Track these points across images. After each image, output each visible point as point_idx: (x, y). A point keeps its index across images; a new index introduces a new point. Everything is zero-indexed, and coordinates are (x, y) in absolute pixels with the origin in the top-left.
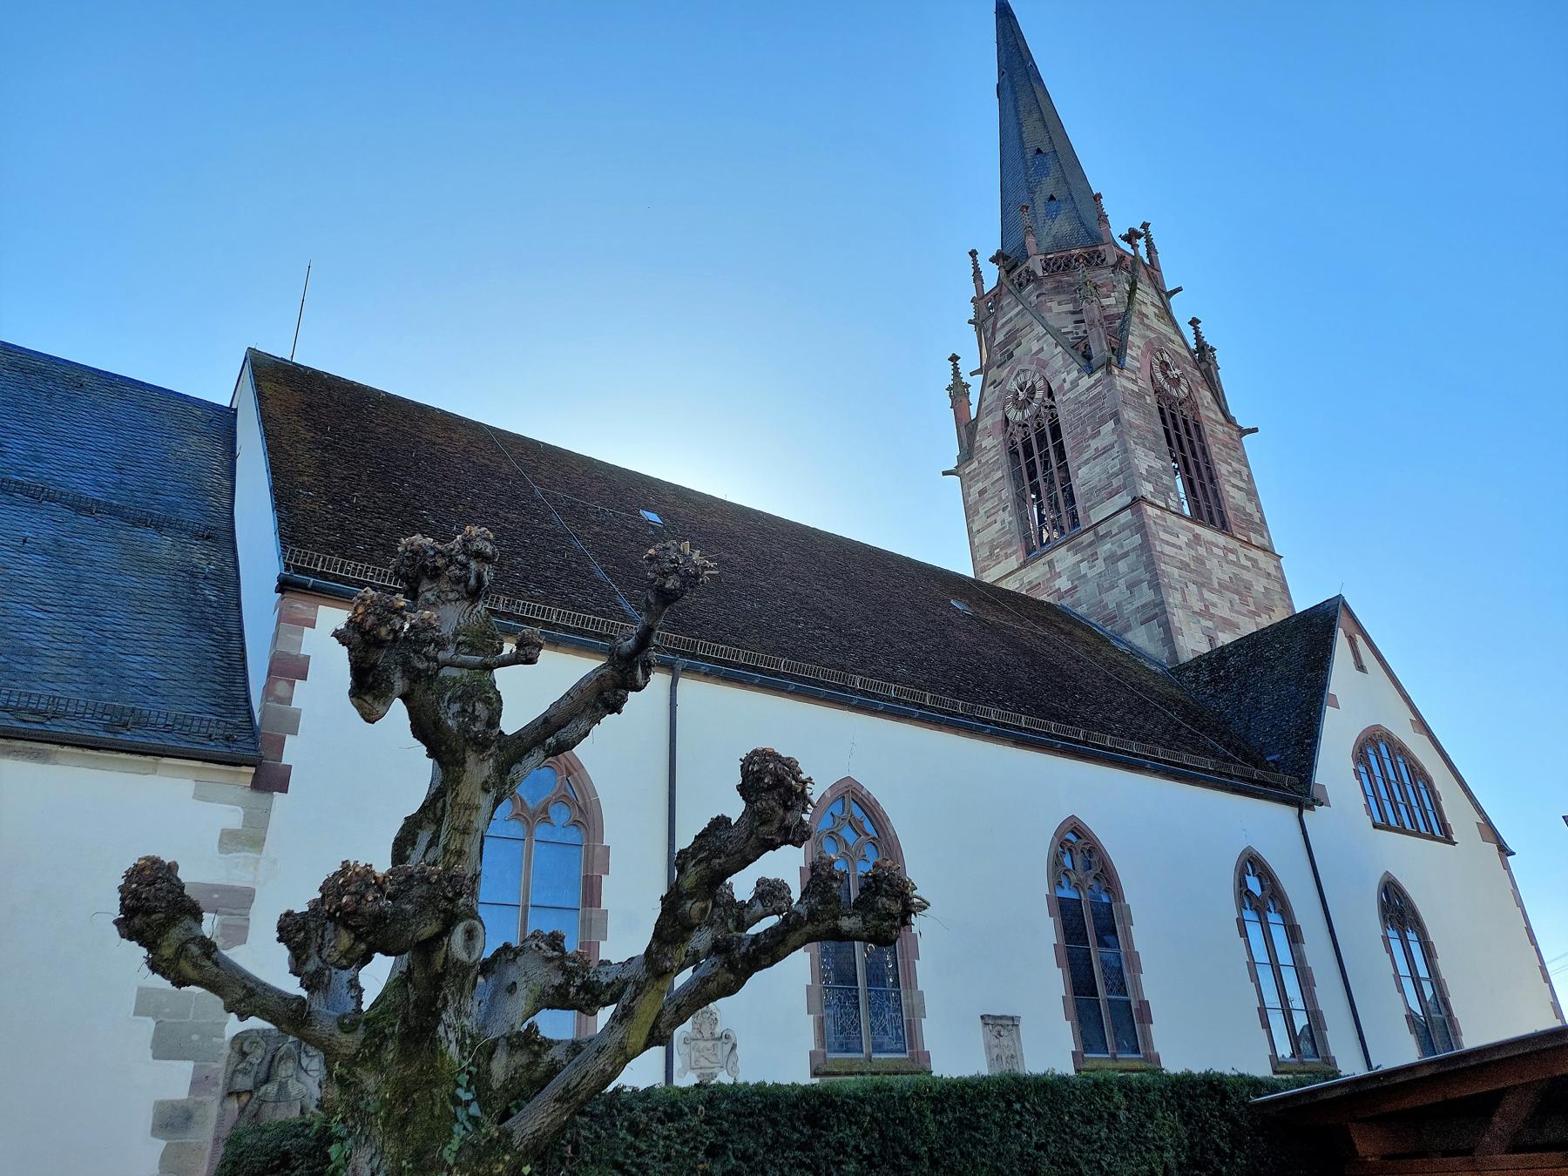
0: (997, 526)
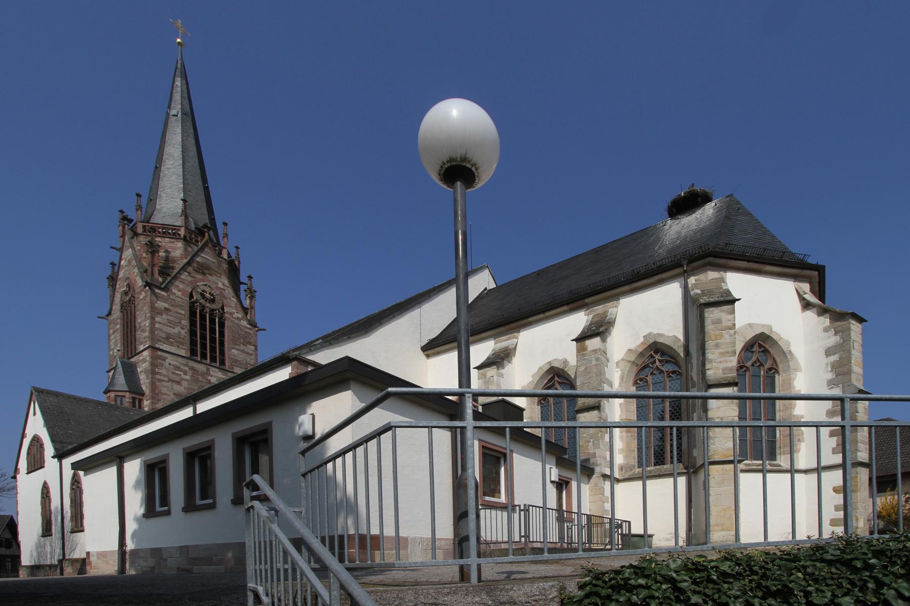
0: (176, 331)
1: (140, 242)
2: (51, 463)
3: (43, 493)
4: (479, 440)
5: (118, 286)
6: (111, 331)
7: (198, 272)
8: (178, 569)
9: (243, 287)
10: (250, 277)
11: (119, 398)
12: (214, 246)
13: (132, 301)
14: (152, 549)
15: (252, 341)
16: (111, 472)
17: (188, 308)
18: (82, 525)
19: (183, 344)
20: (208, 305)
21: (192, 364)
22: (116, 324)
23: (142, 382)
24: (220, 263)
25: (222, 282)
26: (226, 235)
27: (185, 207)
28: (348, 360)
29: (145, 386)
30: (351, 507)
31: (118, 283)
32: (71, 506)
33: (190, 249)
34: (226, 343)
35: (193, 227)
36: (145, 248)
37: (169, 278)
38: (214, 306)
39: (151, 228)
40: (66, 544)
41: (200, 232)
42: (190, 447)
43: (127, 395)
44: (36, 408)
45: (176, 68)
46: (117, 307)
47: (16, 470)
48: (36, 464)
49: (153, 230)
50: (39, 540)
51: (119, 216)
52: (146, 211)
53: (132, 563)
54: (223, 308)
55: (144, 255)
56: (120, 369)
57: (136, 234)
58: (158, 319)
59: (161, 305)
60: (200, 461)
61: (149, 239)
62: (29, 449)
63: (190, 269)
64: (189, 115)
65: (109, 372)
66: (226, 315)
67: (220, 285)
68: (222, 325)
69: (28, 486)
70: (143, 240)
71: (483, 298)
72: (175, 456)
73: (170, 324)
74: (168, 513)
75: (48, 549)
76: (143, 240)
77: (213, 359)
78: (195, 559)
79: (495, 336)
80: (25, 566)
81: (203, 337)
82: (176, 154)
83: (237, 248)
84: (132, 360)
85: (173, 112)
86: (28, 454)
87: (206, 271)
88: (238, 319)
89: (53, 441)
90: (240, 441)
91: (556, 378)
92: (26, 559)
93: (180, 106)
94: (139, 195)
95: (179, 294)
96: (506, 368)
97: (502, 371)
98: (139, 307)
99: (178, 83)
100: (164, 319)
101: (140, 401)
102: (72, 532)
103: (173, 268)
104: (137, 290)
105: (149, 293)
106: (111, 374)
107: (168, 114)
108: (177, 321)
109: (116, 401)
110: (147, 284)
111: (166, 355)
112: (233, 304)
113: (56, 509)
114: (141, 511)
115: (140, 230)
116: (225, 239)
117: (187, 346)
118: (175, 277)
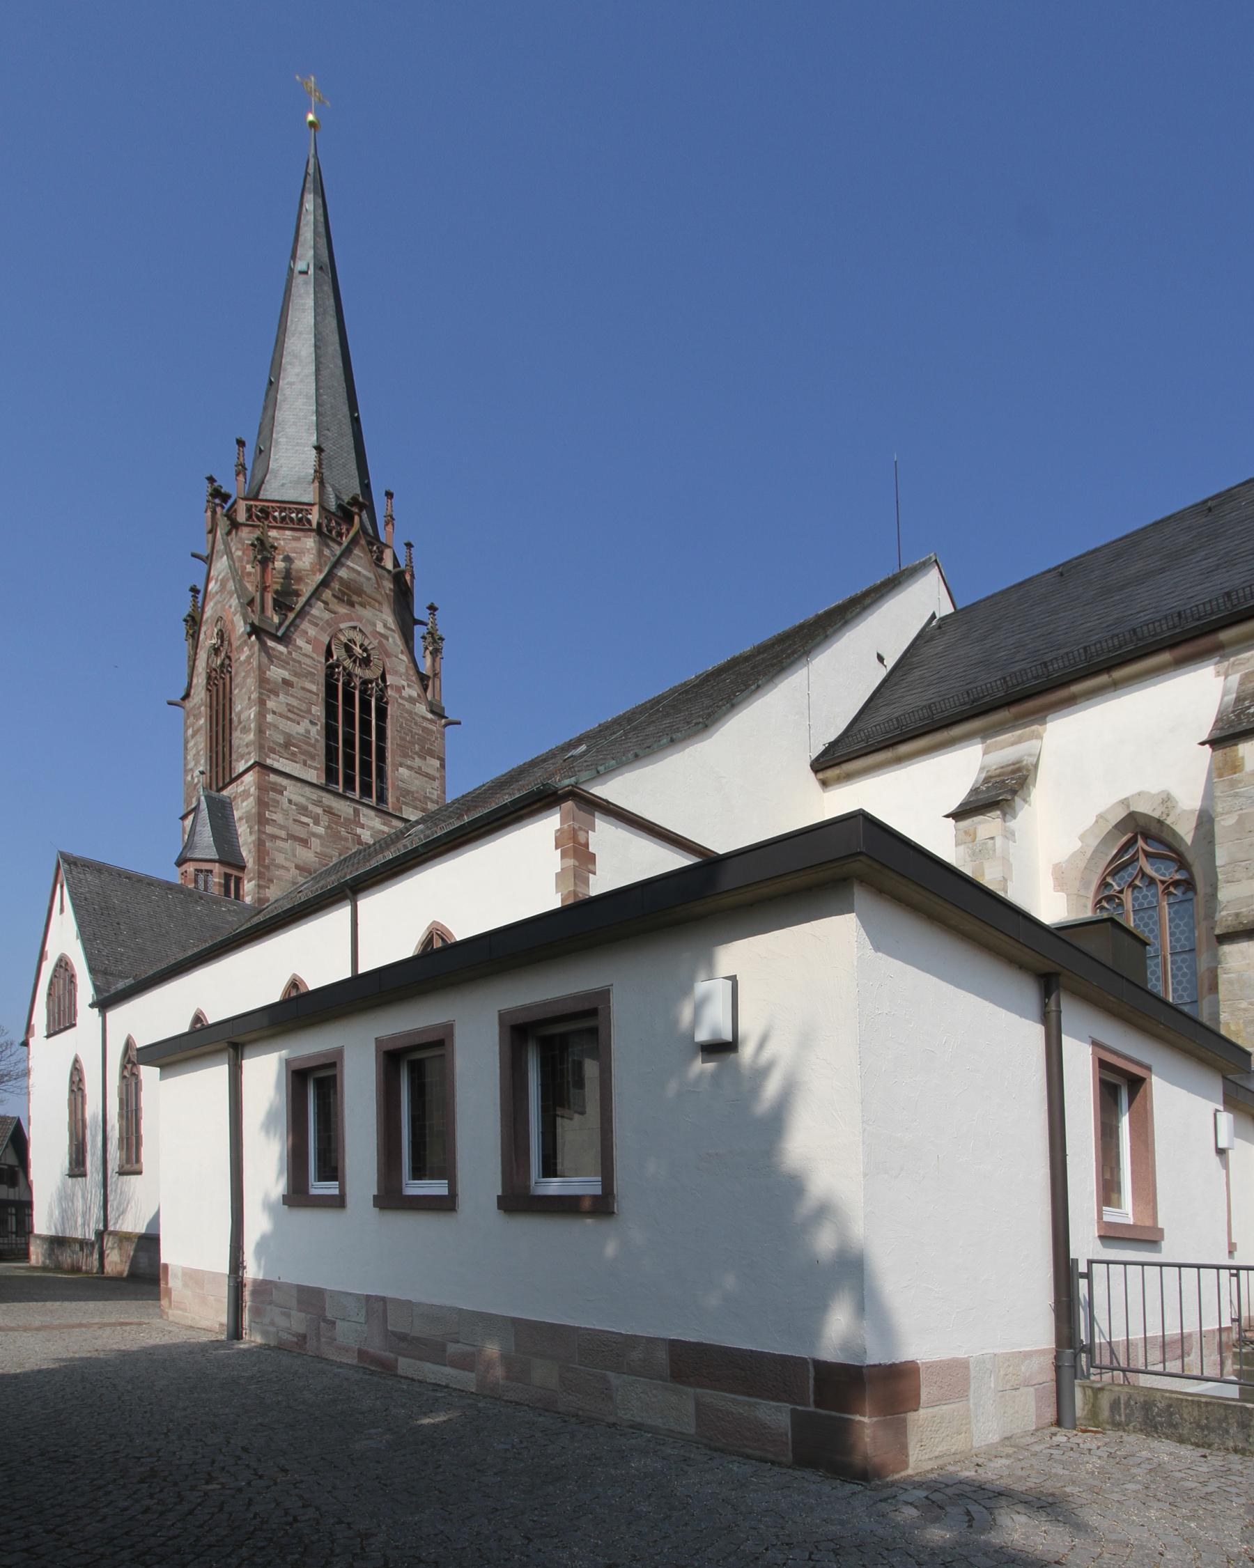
0: (300, 729)
1: (241, 541)
2: (87, 1016)
3: (72, 1082)
4: (1095, 1044)
5: (202, 636)
6: (190, 732)
7: (340, 600)
8: (362, 1354)
9: (419, 631)
10: (432, 608)
11: (201, 876)
12: (370, 544)
13: (225, 668)
14: (302, 1289)
15: (436, 748)
16: (216, 1075)
17: (322, 680)
18: (138, 1160)
19: (313, 757)
20: (358, 671)
21: (328, 800)
22: (197, 717)
23: (241, 840)
24: (379, 578)
25: (383, 620)
26: (390, 519)
27: (320, 462)
28: (861, 818)
29: (247, 854)
30: (851, 1270)
31: (203, 629)
32: (121, 1116)
33: (327, 552)
34: (389, 755)
35: (332, 505)
36: (251, 553)
37: (291, 616)
38: (368, 674)
39: (262, 511)
40: (111, 1198)
41: (345, 514)
42: (393, 1038)
43: (216, 868)
44: (64, 897)
45: (307, 173)
46: (200, 680)
47: (29, 1028)
48: (62, 1021)
49: (266, 513)
50: (64, 1184)
51: (206, 488)
52: (253, 476)
53: (256, 1312)
54: (384, 680)
55: (249, 568)
56: (204, 813)
57: (235, 525)
58: (270, 704)
59: (277, 673)
60: (415, 1072)
61: (257, 533)
62: (51, 983)
63: (327, 595)
64: (328, 269)
65: (184, 818)
66: (390, 692)
67: (380, 628)
68: (382, 714)
69: (48, 1061)
70: (247, 536)
71: (932, 639)
72: (357, 1050)
73: (293, 714)
74: (339, 1202)
75: (79, 1204)
76: (247, 536)
77: (366, 791)
78: (403, 1338)
79: (984, 734)
80: (39, 1237)
81: (349, 743)
82: (304, 353)
83: (409, 545)
84: (225, 793)
85: (300, 265)
86: (49, 995)
87: (355, 598)
88: (411, 700)
89: (92, 970)
90: (520, 1033)
91: (1140, 843)
92: (43, 1222)
93: (311, 253)
94: (241, 443)
95: (308, 648)
96: (1020, 815)
97: (1013, 824)
98: (237, 680)
99: (309, 205)
100: (282, 709)
101: (238, 881)
102: (121, 1173)
103: (297, 594)
104: (236, 644)
105: (256, 648)
106: (188, 822)
107: (291, 270)
108: (304, 707)
109: (196, 881)
110: (255, 630)
111: (285, 782)
112: (402, 670)
113: (94, 1117)
114: (278, 1187)
115: (242, 517)
116: (390, 527)
117: (320, 762)
118: (301, 614)
